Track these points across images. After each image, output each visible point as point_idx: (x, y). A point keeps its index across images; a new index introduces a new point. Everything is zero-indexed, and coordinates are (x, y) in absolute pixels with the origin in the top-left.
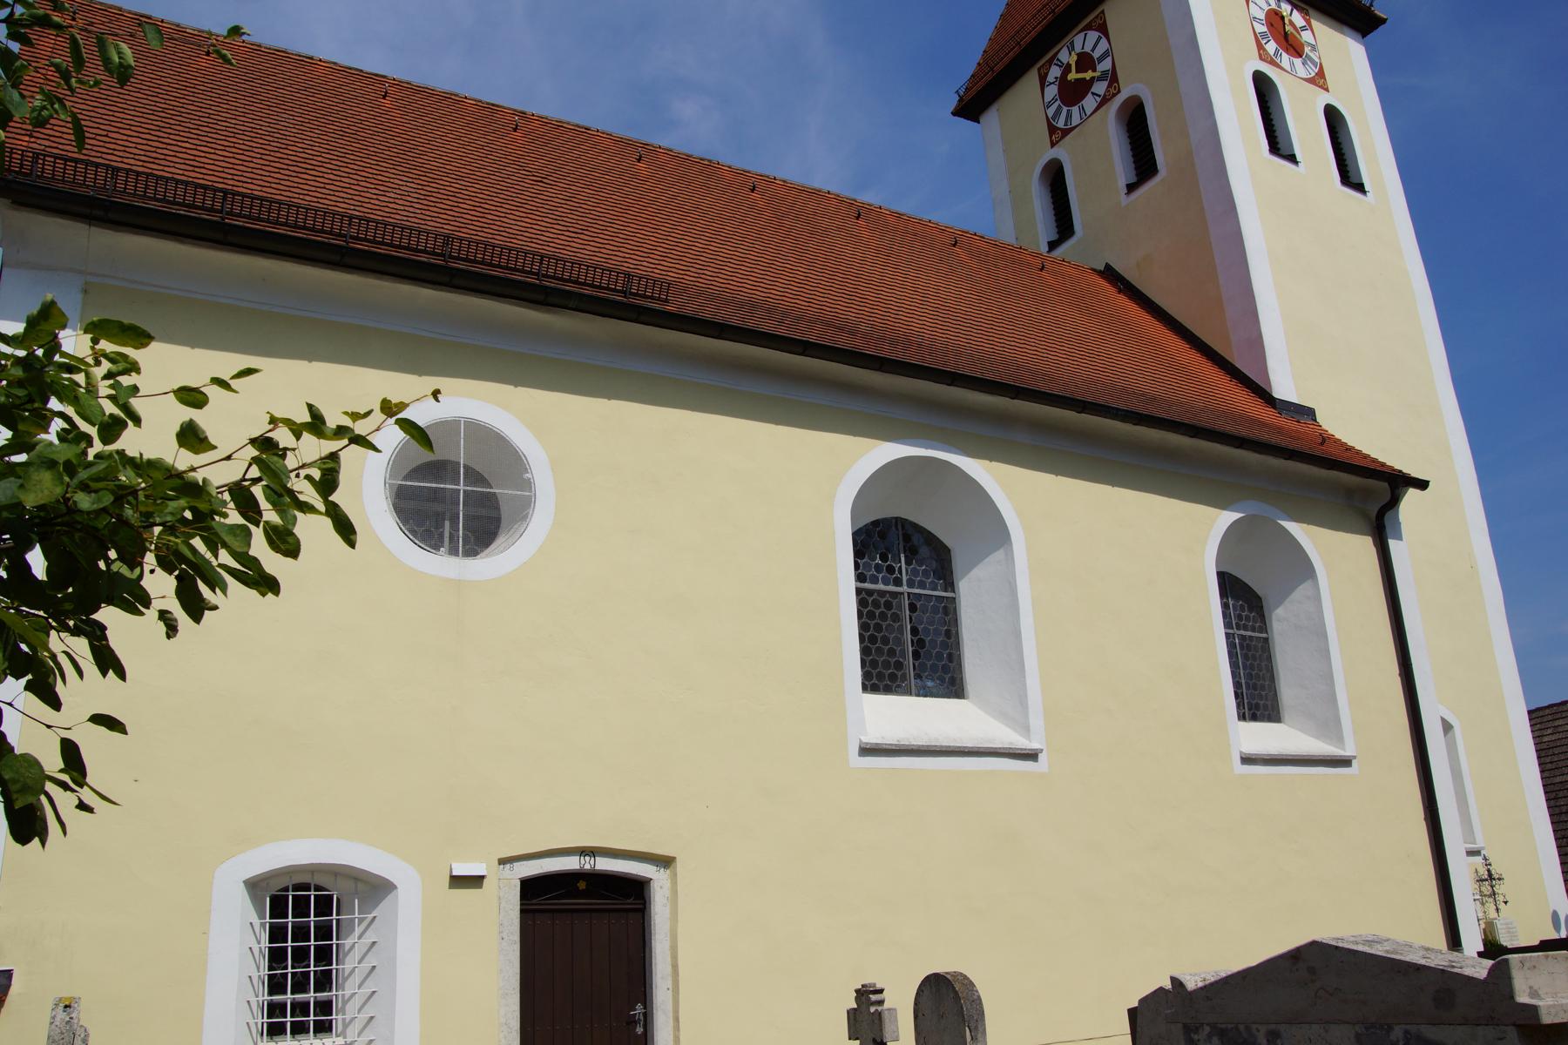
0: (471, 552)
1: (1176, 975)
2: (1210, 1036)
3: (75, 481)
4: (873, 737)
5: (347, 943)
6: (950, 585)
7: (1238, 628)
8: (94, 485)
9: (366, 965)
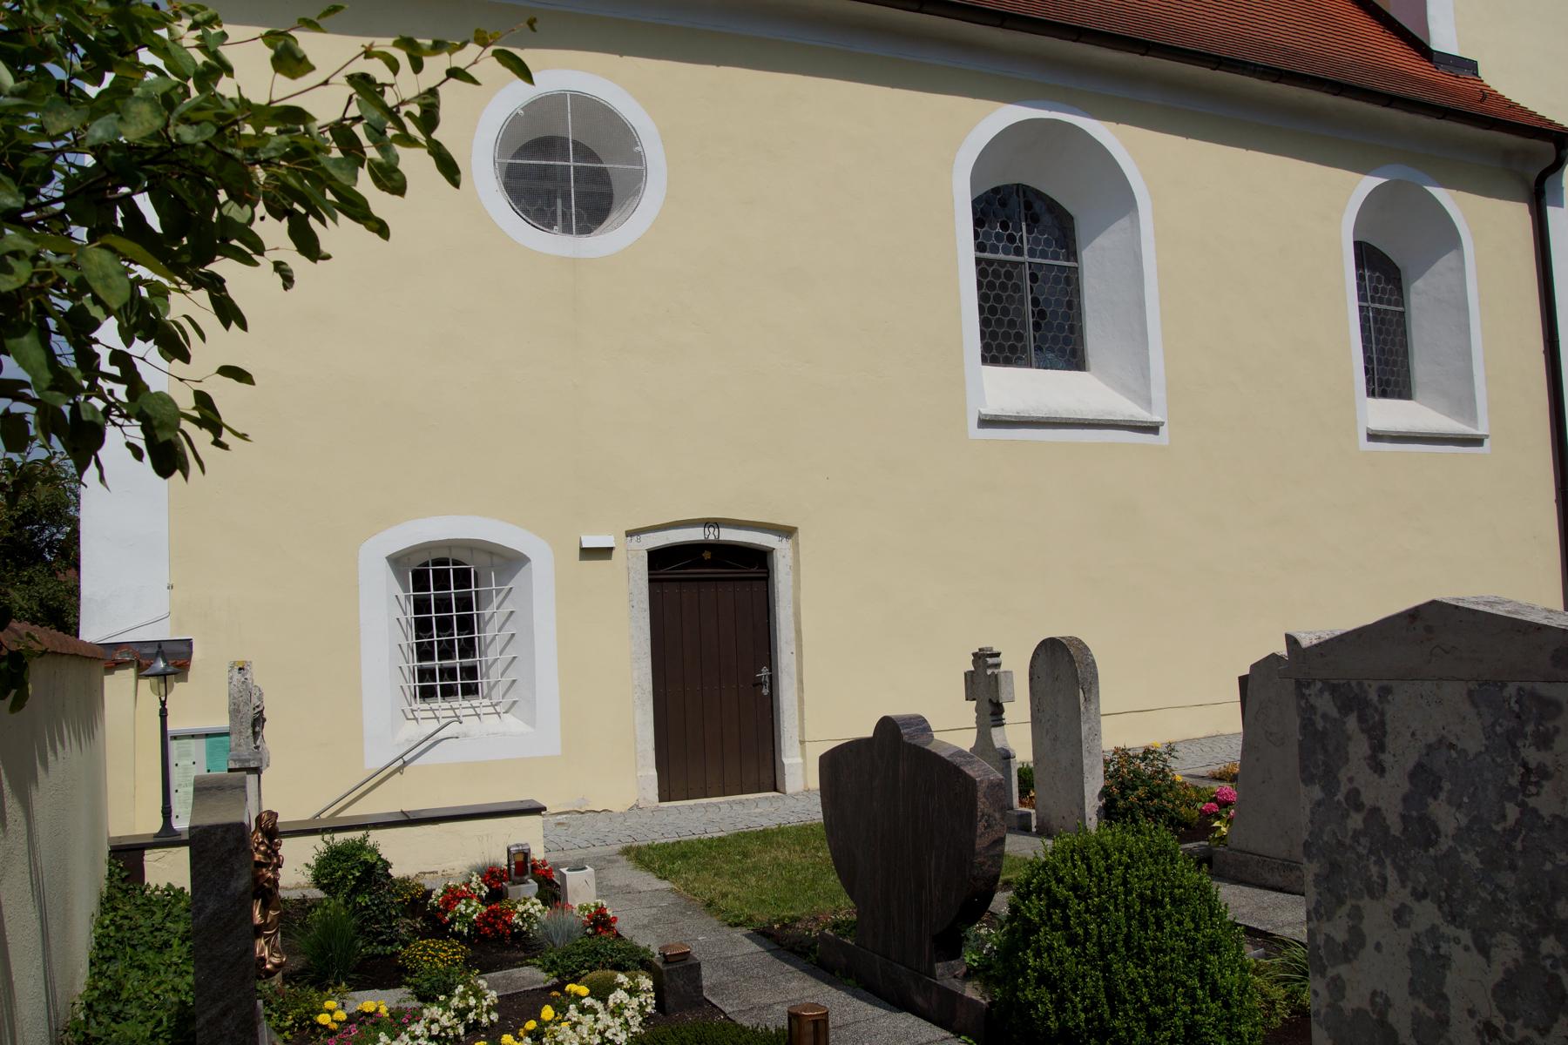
0: (585, 230)
1: (1291, 632)
2: (1321, 691)
3: (175, 115)
4: (992, 409)
5: (487, 612)
6: (1073, 254)
7: (1373, 301)
8: (195, 116)
9: (506, 633)
